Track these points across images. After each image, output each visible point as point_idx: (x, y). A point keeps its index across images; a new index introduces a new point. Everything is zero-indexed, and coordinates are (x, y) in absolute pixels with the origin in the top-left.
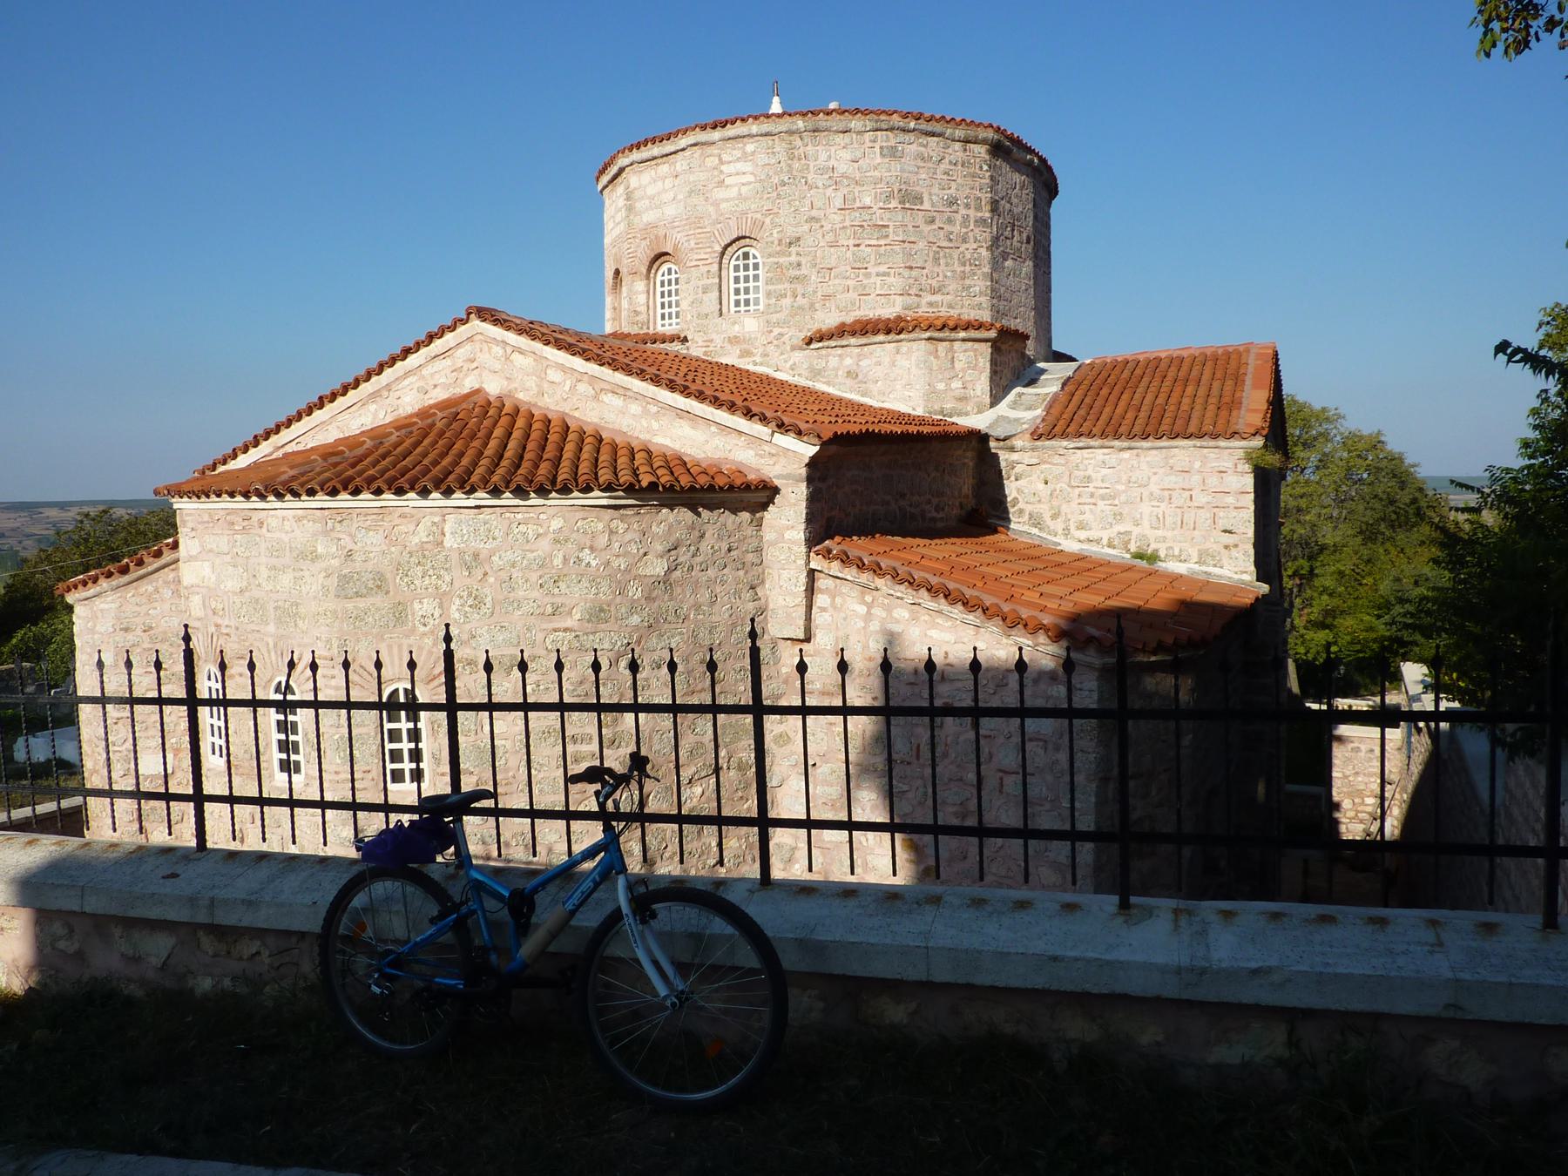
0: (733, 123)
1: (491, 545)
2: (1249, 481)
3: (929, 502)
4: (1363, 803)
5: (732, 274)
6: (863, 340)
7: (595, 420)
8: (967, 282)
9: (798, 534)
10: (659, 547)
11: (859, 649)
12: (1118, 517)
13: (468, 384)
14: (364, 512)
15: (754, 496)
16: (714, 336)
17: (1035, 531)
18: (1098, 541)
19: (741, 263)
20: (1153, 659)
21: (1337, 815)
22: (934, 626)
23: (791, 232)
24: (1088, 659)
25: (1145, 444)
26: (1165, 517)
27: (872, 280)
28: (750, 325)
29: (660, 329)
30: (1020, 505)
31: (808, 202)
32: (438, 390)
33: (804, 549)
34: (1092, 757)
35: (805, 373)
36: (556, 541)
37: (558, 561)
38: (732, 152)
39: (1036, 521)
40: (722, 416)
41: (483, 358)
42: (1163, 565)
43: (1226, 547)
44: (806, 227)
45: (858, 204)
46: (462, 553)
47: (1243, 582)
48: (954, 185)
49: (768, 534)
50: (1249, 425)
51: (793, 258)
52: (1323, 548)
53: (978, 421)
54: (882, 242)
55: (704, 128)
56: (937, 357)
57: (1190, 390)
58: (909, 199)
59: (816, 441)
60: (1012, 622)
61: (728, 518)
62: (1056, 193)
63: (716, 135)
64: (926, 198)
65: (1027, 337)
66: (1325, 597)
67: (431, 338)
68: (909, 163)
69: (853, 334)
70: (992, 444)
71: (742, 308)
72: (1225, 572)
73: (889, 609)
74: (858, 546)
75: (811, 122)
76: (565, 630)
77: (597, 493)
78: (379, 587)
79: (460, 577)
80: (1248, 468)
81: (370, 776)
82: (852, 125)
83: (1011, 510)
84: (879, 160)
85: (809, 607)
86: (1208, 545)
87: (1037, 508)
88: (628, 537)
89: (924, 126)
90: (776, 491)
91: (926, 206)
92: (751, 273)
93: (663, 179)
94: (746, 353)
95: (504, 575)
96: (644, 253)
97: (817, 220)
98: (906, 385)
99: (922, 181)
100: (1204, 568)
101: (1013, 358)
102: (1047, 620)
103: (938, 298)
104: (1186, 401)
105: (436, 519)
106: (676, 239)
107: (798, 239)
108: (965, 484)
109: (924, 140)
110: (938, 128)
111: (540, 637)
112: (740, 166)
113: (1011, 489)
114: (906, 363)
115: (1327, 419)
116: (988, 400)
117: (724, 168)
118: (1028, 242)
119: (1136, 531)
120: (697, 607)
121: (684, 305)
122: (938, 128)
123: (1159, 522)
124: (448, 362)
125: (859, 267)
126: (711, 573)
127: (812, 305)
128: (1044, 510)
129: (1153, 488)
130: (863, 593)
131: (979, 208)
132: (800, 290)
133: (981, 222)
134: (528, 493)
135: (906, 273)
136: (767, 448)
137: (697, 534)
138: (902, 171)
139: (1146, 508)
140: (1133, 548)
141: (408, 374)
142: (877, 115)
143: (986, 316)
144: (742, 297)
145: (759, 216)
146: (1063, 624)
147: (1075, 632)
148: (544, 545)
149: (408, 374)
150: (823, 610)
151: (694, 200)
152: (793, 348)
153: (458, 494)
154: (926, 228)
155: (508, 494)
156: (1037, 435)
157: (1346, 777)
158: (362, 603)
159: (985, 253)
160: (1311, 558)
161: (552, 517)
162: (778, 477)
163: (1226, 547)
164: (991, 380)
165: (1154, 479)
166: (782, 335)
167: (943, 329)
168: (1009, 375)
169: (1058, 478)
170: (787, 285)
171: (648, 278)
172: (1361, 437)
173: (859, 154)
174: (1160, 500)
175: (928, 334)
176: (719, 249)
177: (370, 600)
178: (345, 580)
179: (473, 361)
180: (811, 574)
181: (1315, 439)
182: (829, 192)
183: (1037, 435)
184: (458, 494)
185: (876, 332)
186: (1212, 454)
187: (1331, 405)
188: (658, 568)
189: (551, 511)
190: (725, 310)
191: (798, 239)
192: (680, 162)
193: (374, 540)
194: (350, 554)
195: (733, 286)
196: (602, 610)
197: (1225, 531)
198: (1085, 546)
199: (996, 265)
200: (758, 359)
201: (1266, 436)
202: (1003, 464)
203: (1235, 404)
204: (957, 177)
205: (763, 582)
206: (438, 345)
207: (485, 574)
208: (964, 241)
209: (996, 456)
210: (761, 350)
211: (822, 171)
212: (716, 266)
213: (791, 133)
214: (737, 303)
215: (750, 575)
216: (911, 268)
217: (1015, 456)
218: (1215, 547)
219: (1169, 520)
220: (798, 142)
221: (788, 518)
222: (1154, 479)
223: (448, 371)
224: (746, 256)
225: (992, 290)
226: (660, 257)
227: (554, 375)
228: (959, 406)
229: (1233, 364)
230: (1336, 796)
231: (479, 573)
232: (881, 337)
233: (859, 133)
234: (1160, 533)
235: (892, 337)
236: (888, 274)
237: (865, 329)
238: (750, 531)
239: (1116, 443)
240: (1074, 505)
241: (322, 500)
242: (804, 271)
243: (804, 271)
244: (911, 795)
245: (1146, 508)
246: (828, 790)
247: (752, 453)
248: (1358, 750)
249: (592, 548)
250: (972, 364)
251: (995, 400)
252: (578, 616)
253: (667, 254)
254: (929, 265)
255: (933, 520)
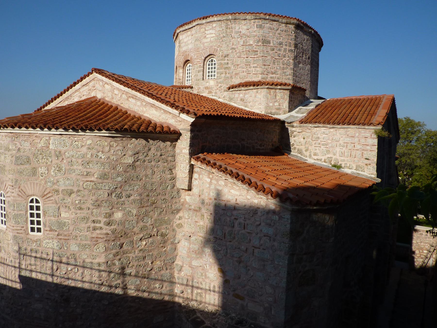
0: (209, 17)
1: (65, 148)
2: (376, 141)
3: (257, 143)
4: (423, 252)
5: (208, 67)
6: (246, 88)
7: (127, 107)
8: (285, 71)
9: (186, 151)
10: (130, 153)
11: (207, 195)
12: (328, 152)
13: (93, 95)
14: (24, 135)
15: (173, 136)
16: (201, 87)
17: (299, 155)
18: (321, 160)
19: (210, 63)
20: (315, 208)
21: (414, 255)
22: (233, 188)
23: (226, 53)
24: (286, 206)
25: (338, 126)
26: (345, 153)
27: (251, 69)
28: (212, 83)
29: (186, 84)
30: (295, 146)
31: (232, 43)
32: (84, 97)
33: (188, 157)
34: (287, 245)
35: (228, 99)
36: (89, 148)
37: (89, 156)
38: (209, 27)
39: (300, 152)
40: (163, 106)
41: (97, 86)
42: (343, 170)
43: (366, 165)
44: (231, 51)
45: (248, 44)
46: (55, 151)
47: (371, 178)
48: (281, 38)
49: (177, 150)
50: (377, 121)
51: (226, 61)
52: (416, 166)
53: (282, 117)
54: (256, 56)
55: (200, 19)
56: (270, 94)
57: (360, 108)
58: (266, 42)
59: (194, 116)
60: (261, 189)
61: (161, 144)
62: (322, 45)
63: (204, 21)
64: (271, 42)
65: (305, 90)
66: (416, 182)
67: (82, 79)
68: (266, 30)
69: (243, 86)
70: (286, 124)
71: (210, 78)
72: (365, 174)
73: (217, 181)
74: (211, 157)
75: (234, 16)
76: (91, 181)
77: (104, 131)
78: (28, 162)
79: (54, 159)
80: (375, 136)
81: (23, 229)
82: (247, 17)
83: (292, 148)
84: (256, 29)
85: (191, 178)
86: (360, 164)
87: (300, 147)
88: (118, 148)
89: (272, 18)
90: (180, 134)
91: (271, 44)
92: (213, 66)
93: (189, 36)
94: (210, 92)
95: (69, 160)
96: (183, 61)
97: (234, 49)
98: (256, 103)
99: (270, 36)
100: (358, 172)
101: (298, 96)
102: (274, 189)
103: (274, 75)
104: (357, 112)
105: (47, 138)
106: (192, 55)
107: (228, 55)
108: (275, 138)
109: (271, 23)
110: (276, 18)
111: (81, 183)
112: (211, 31)
113: (292, 140)
114: (260, 96)
115: (420, 126)
116: (288, 110)
117: (206, 32)
118: (309, 58)
119: (334, 157)
120: (146, 176)
121: (193, 76)
122: (276, 18)
123: (342, 154)
124: (87, 87)
125: (248, 64)
126: (153, 163)
127: (231, 77)
128: (303, 148)
129: (341, 142)
130: (209, 174)
131: (290, 46)
132: (228, 71)
133: (291, 51)
134: (78, 130)
135: (263, 67)
136: (178, 119)
137: (147, 149)
138: (263, 33)
139: (338, 149)
140: (333, 163)
141: (76, 91)
142: (256, 14)
143: (291, 82)
144: (210, 74)
145: (216, 47)
146: (280, 191)
147: (282, 196)
148: (84, 150)
149: (76, 91)
150: (196, 179)
151: (197, 43)
152: (225, 91)
153: (53, 130)
154: (271, 52)
155: (71, 130)
156: (301, 122)
157: (417, 243)
158: (22, 167)
159: (291, 61)
160: (412, 169)
161: (88, 139)
162: (181, 129)
163: (366, 165)
164: (289, 103)
165: (341, 139)
166: (221, 86)
167: (272, 85)
168: (298, 102)
169: (308, 137)
170: (223, 70)
171: (183, 68)
172: (431, 132)
173: (249, 27)
174: (343, 146)
175: (267, 87)
176: (203, 58)
177: (25, 166)
178: (17, 158)
179: (94, 87)
180: (192, 167)
181: (415, 132)
182: (239, 39)
183: (301, 122)
184: (53, 130)
185: (250, 86)
186: (362, 131)
187: (422, 121)
188: (130, 160)
189: (87, 137)
190: (205, 78)
191: (228, 55)
192: (193, 31)
193: (27, 145)
194: (19, 149)
195: (207, 70)
196: (105, 175)
197: (366, 159)
198: (316, 161)
199: (295, 65)
200: (214, 94)
201: (383, 126)
202: (290, 132)
203: (374, 114)
204: (283, 35)
205: (175, 168)
206: (84, 81)
207: (63, 159)
208: (284, 57)
209: (287, 129)
210: (214, 91)
211: (237, 33)
212: (202, 64)
213: (227, 20)
214: (209, 76)
215: (169, 165)
216: (265, 65)
217: (294, 129)
218: (362, 164)
219: (346, 154)
220: (229, 23)
221: (183, 146)
222: (341, 139)
223: (87, 90)
224: (212, 61)
225: (294, 74)
226: (187, 61)
227: (116, 92)
228: (277, 111)
229: (377, 101)
230: (414, 249)
231: (60, 159)
232: (252, 87)
233: (250, 20)
234: (343, 158)
235: (255, 87)
236: (257, 67)
237: (247, 85)
238: (170, 149)
239: (328, 126)
240: (313, 147)
241: (10, 130)
242: (229, 65)
243: (229, 65)
244: (222, 252)
245: (338, 149)
246: (194, 246)
247: (174, 120)
248: (422, 234)
249: (103, 152)
250: (282, 98)
251: (290, 110)
252: (96, 177)
253: (189, 60)
254: (271, 65)
255: (259, 149)
